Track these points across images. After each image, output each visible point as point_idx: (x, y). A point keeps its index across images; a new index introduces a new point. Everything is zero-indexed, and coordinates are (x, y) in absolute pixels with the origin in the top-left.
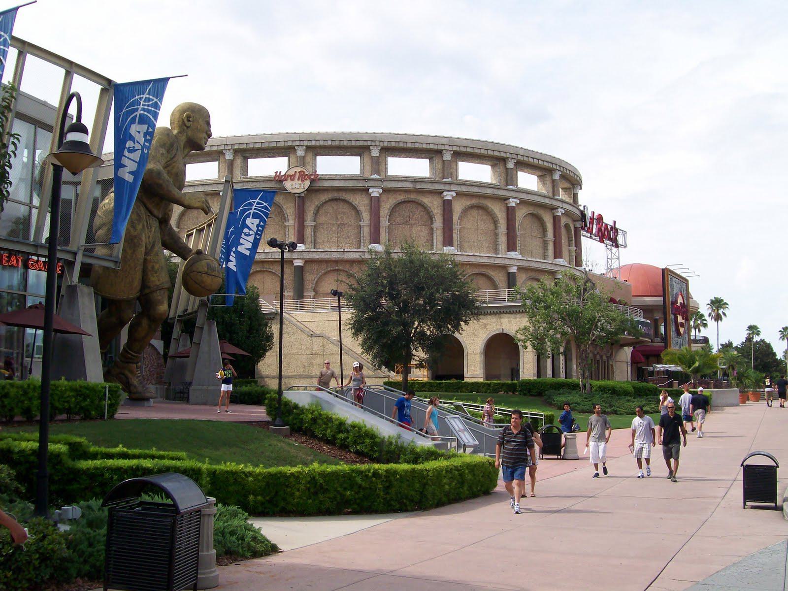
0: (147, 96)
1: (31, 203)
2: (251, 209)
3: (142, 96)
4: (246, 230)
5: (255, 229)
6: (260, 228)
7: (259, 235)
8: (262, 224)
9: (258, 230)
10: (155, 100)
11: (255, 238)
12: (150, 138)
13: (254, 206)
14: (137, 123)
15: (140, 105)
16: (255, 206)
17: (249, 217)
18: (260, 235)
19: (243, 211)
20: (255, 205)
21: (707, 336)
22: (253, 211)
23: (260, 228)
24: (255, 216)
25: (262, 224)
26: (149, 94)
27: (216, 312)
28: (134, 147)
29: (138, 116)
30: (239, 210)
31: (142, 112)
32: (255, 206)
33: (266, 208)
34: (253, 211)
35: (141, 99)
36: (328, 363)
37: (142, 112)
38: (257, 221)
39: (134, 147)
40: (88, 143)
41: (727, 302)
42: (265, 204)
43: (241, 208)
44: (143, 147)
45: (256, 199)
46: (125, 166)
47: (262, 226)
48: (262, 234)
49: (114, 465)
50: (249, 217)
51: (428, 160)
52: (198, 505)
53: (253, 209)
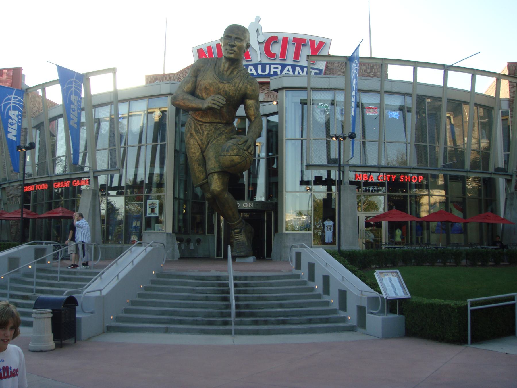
1: (406, 141)
2: (10, 103)
4: (10, 121)
5: (16, 119)
6: (19, 117)
9: (19, 119)
11: (18, 125)
16: (13, 101)
18: (21, 123)
19: (6, 105)
20: (12, 99)
21: (250, 22)
22: (12, 104)
23: (19, 117)
24: (15, 108)
27: (224, 93)
28: (13, 123)
30: (2, 105)
32: (13, 101)
33: (20, 101)
34: (12, 104)
36: (3, 361)
39: (13, 123)
40: (279, 233)
42: (19, 98)
43: (3, 103)
44: (18, 122)
45: (12, 94)
46: (10, 132)
48: (18, 120)
50: (11, 110)
53: (12, 103)
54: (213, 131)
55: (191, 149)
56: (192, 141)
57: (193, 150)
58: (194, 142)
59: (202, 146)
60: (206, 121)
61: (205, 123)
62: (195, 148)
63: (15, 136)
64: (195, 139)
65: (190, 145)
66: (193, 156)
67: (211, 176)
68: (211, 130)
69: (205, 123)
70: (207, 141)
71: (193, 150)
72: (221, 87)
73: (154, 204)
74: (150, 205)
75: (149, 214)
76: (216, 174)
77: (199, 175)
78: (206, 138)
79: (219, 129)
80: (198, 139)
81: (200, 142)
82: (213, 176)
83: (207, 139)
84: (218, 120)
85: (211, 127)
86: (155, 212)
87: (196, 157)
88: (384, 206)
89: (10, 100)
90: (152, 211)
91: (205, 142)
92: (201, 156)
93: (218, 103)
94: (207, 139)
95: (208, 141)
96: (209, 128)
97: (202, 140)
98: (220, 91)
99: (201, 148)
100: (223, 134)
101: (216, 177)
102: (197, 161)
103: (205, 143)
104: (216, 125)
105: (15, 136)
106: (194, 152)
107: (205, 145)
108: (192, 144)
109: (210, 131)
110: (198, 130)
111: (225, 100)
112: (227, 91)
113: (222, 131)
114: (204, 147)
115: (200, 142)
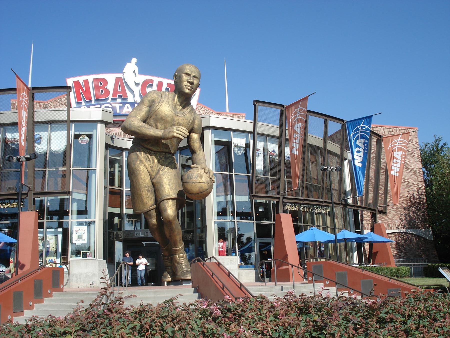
0: (400, 139)
2: (396, 146)
3: (398, 140)
5: (363, 147)
6: (366, 145)
7: (366, 150)
8: (366, 141)
9: (365, 146)
10: (367, 127)
12: (367, 145)
13: (360, 130)
14: (359, 139)
15: (359, 130)
17: (358, 139)
22: (397, 147)
23: (366, 145)
24: (400, 150)
25: (366, 141)
26: (400, 139)
29: (359, 136)
31: (398, 147)
32: (361, 130)
35: (297, 110)
37: (398, 147)
38: (363, 141)
39: (360, 150)
41: (136, 295)
47: (367, 143)
49: (194, 143)
51: (105, 125)
52: (5, 289)
53: (360, 132)
54: (163, 160)
55: (141, 175)
56: (142, 168)
57: (142, 177)
58: (144, 169)
59: (152, 173)
60: (157, 150)
61: (155, 151)
62: (145, 175)
63: (360, 162)
64: (145, 166)
65: (139, 172)
66: (142, 183)
67: (165, 201)
68: (162, 159)
69: (155, 151)
70: (157, 169)
71: (142, 177)
72: (176, 119)
73: (82, 230)
74: (76, 231)
75: (76, 240)
76: (170, 200)
77: (148, 201)
78: (157, 166)
79: (168, 158)
80: (148, 167)
81: (150, 169)
82: (167, 202)
83: (157, 167)
84: (168, 150)
85: (161, 156)
86: (83, 238)
87: (145, 183)
88: (345, 225)
89: (358, 130)
90: (80, 237)
91: (156, 170)
92: (151, 183)
93: (183, 134)
94: (157, 167)
95: (158, 168)
96: (159, 157)
97: (152, 167)
98: (174, 123)
99: (150, 175)
100: (172, 163)
101: (170, 202)
102: (147, 188)
103: (155, 171)
104: (165, 155)
105: (360, 162)
106: (144, 178)
107: (155, 172)
108: (142, 170)
109: (160, 159)
110: (147, 157)
111: (188, 131)
112: (181, 123)
113: (171, 160)
114: (154, 174)
115: (150, 169)
